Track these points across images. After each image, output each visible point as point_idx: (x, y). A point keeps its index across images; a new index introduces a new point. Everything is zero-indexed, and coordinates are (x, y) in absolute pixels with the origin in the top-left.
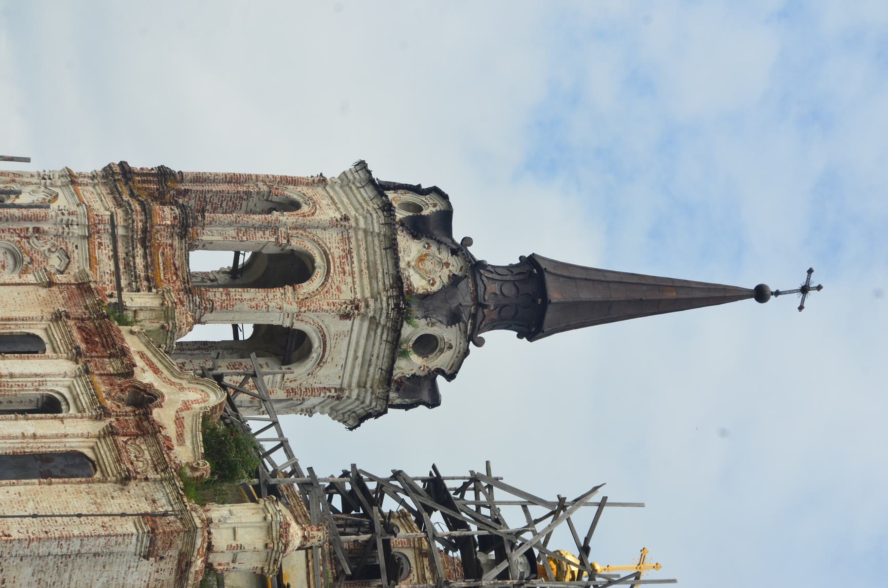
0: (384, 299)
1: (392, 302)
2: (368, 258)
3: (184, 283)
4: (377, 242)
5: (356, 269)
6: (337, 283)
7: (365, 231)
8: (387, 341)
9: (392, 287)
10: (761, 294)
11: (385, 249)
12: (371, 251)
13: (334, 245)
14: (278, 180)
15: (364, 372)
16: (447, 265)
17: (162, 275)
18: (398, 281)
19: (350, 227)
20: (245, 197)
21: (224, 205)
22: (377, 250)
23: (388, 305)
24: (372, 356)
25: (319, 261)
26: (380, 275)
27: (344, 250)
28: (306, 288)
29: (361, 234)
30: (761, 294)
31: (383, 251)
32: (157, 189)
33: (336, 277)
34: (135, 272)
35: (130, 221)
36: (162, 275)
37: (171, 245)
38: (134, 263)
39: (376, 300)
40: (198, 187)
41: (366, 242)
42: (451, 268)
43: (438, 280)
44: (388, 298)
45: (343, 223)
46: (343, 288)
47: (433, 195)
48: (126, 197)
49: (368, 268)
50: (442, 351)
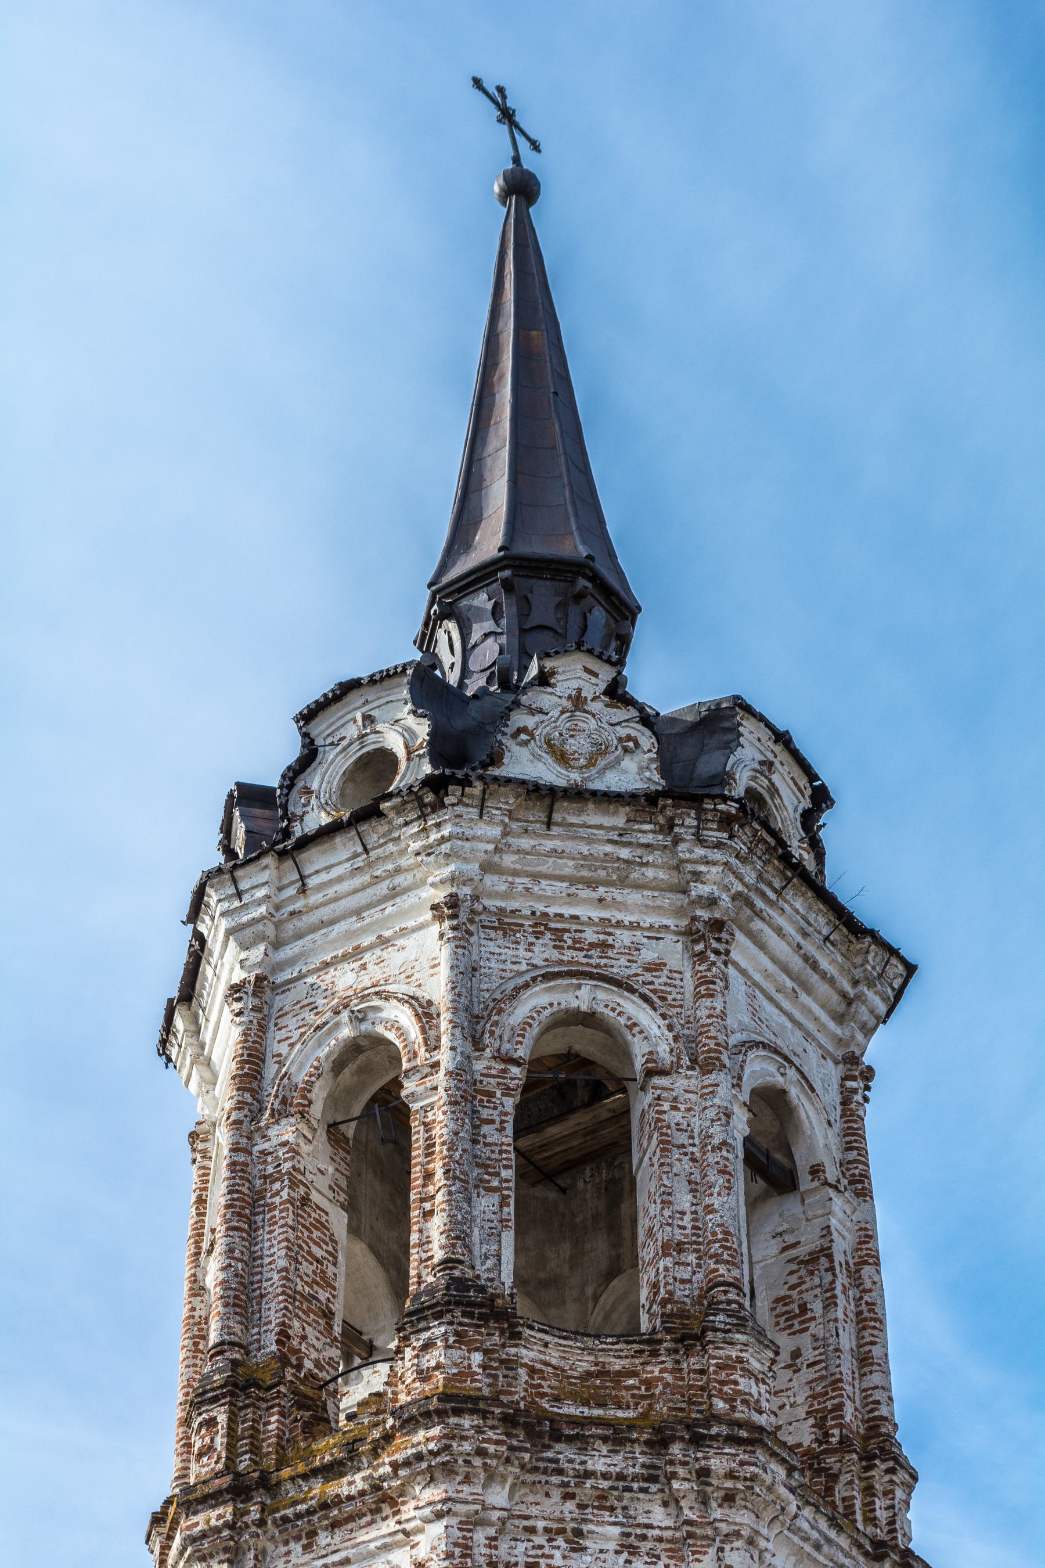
0: (700, 852)
1: (713, 835)
2: (561, 878)
3: (655, 1353)
4: (526, 843)
5: (596, 914)
6: (634, 969)
7: (487, 868)
8: (778, 893)
9: (669, 827)
10: (521, 188)
11: (549, 824)
12: (547, 866)
13: (522, 952)
14: (248, 1097)
15: (823, 989)
16: (578, 701)
17: (620, 1414)
18: (643, 803)
19: (476, 898)
20: (302, 1190)
21: (318, 1252)
22: (549, 844)
23: (719, 845)
24: (799, 947)
25: (583, 997)
26: (625, 853)
27: (538, 935)
28: (650, 1034)
29: (491, 880)
30: (521, 188)
31: (555, 830)
32: (282, 1414)
33: (619, 967)
34: (635, 1478)
35: (477, 1462)
36: (620, 1414)
37: (532, 1371)
38: (605, 1476)
39: (697, 876)
40: (273, 1312)
41: (516, 873)
42: (587, 693)
43: (622, 732)
44: (700, 841)
45: (463, 917)
46: (648, 955)
47: (319, 729)
48: (353, 1483)
49: (592, 884)
50: (774, 790)
